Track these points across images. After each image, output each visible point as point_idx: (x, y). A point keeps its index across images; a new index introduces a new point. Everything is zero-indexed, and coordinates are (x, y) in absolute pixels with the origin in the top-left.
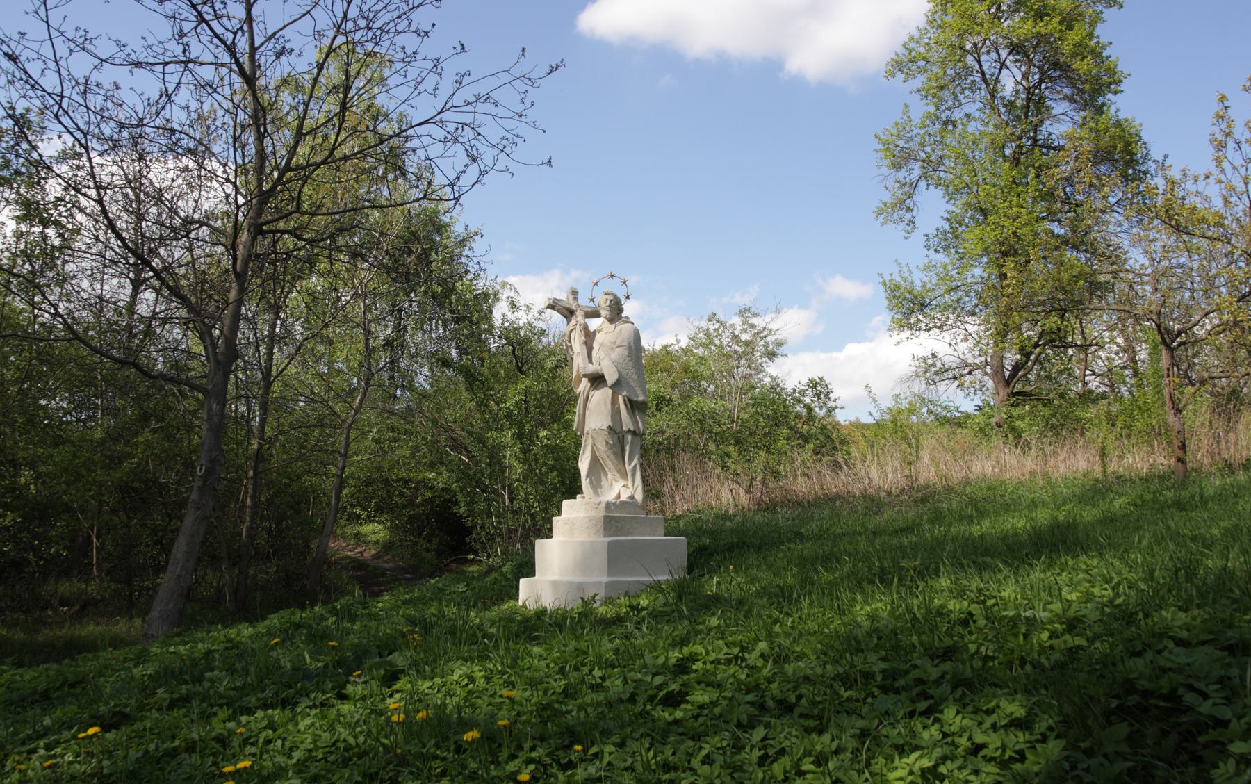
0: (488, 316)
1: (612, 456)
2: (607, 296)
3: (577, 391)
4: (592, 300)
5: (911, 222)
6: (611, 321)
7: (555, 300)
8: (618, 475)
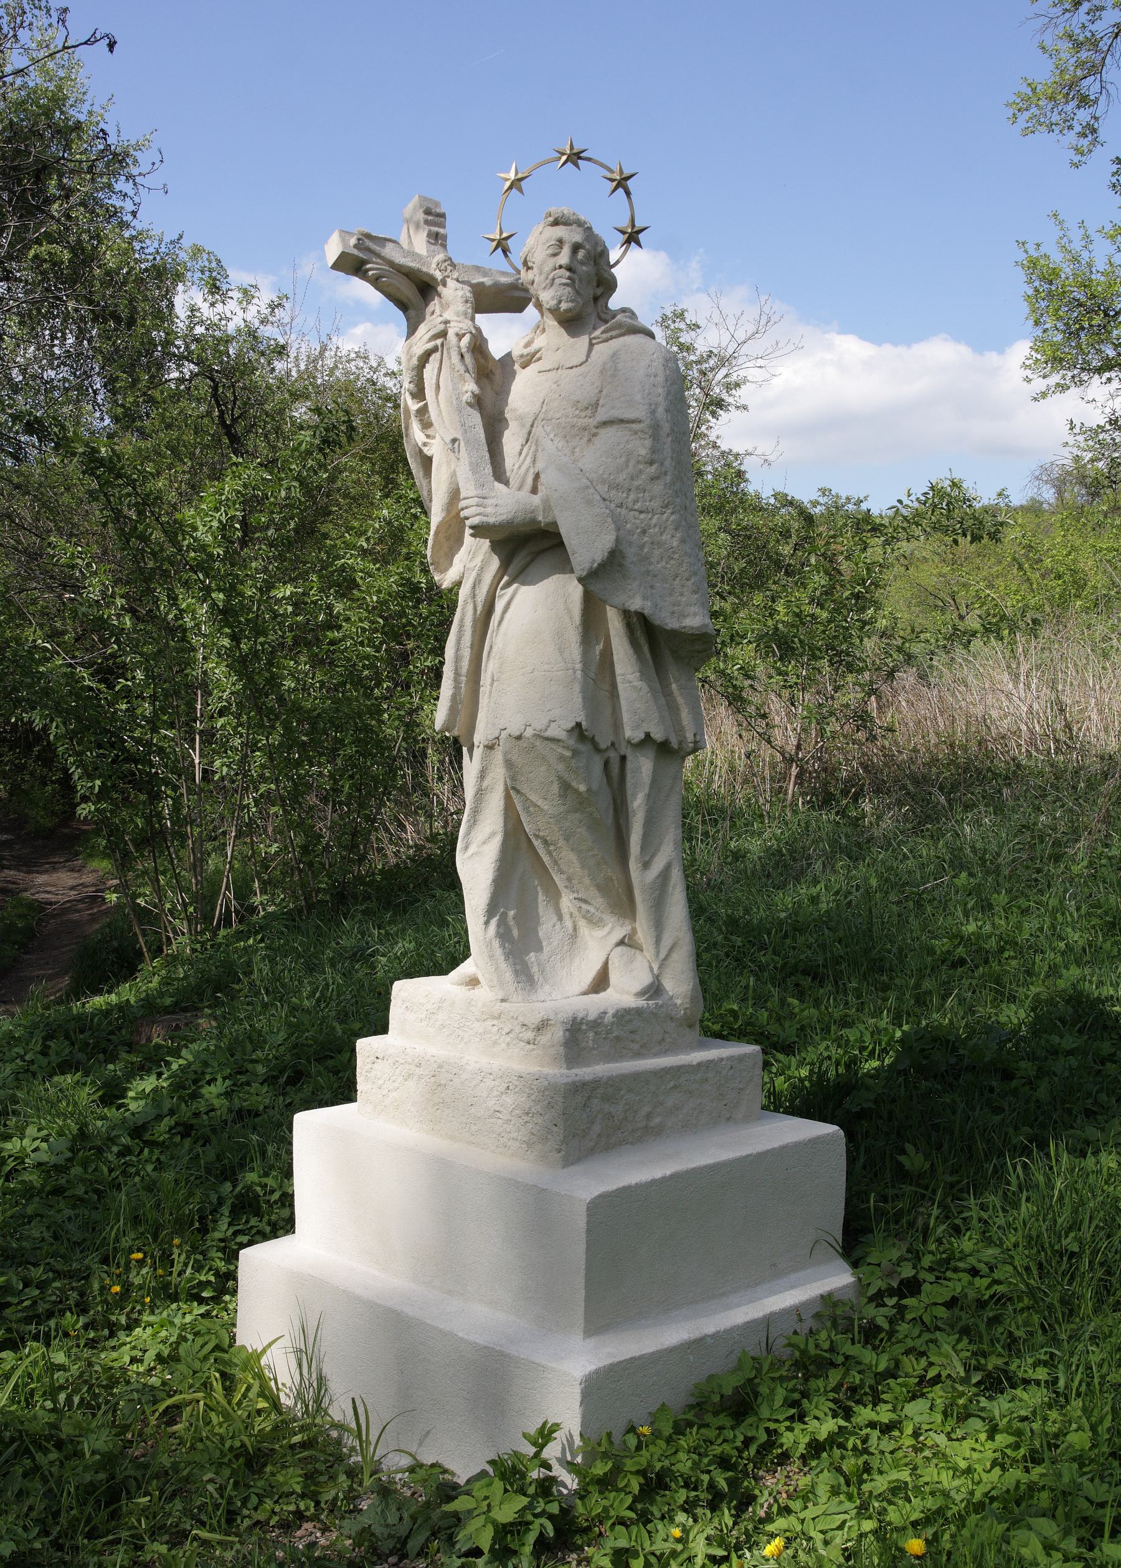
0: (163, 316)
1: (582, 831)
2: (560, 231)
3: (446, 580)
4: (502, 246)
5: (1090, 130)
6: (572, 322)
7: (367, 241)
8: (599, 901)
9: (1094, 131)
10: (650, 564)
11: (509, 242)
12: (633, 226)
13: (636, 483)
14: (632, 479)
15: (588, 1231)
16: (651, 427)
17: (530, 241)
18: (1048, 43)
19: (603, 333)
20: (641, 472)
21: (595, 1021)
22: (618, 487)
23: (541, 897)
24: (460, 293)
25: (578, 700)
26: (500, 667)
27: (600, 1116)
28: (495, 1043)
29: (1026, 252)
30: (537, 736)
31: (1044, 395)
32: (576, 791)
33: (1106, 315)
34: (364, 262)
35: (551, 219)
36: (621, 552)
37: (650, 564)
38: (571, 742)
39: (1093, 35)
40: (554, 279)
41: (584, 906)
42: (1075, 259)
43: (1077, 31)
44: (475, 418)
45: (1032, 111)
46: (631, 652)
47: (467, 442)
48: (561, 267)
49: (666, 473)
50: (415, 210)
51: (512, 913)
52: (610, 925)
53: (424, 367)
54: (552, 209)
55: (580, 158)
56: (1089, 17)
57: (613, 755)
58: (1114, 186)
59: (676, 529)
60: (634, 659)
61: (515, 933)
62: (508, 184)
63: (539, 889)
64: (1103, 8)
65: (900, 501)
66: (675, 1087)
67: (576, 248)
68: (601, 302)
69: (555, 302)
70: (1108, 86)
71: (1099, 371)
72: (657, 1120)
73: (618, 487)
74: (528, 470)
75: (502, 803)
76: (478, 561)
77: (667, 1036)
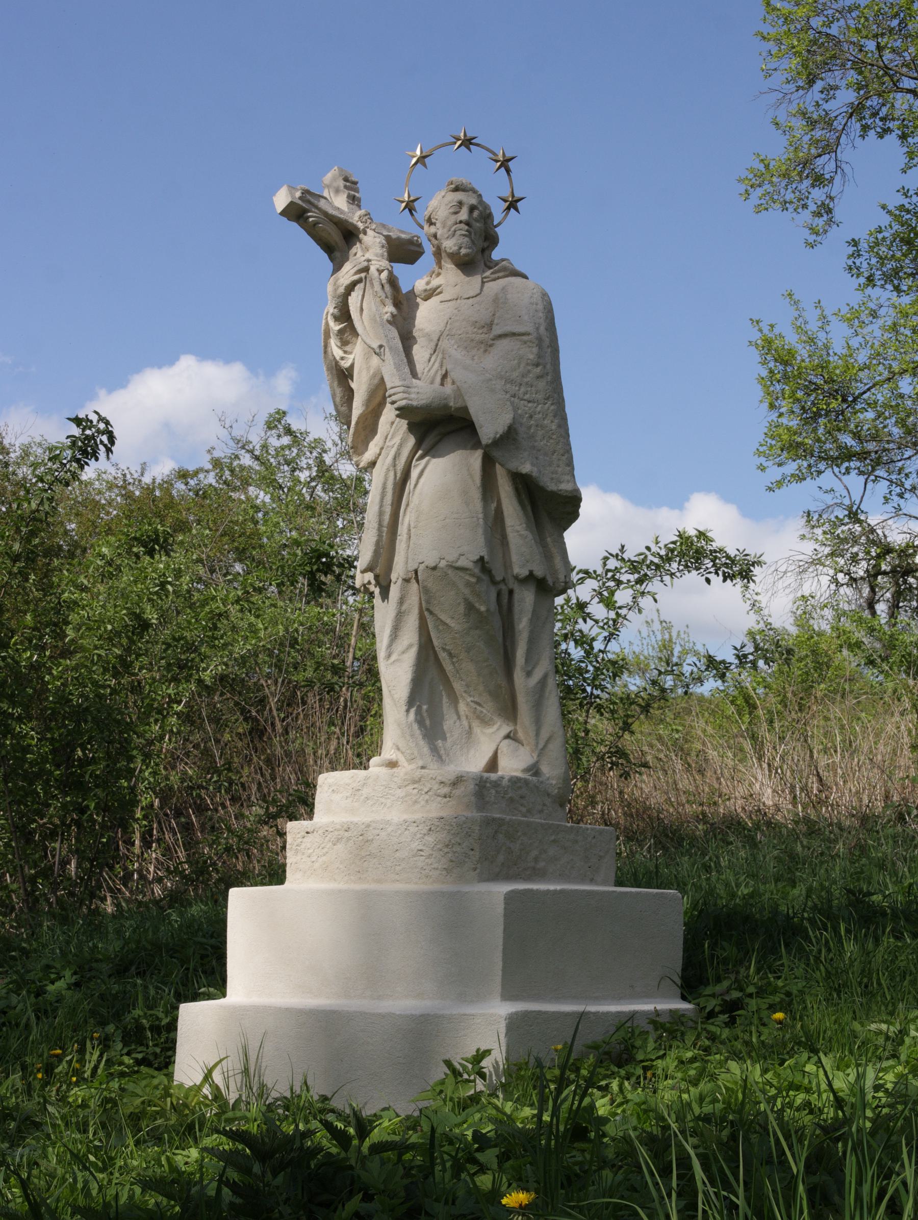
2: (460, 196)
5: (825, 210)
6: (466, 265)
9: (829, 211)
10: (535, 441)
11: (416, 204)
12: (513, 196)
13: (525, 380)
14: (523, 376)
15: (505, 915)
16: (537, 339)
17: (433, 203)
18: (781, 119)
19: (492, 273)
20: (529, 372)
21: (495, 782)
22: (512, 382)
23: (445, 700)
24: (378, 240)
25: (481, 540)
26: (417, 518)
27: (504, 848)
28: (416, 802)
29: (760, 331)
30: (451, 566)
31: (779, 483)
32: (478, 611)
33: (844, 400)
34: (306, 211)
35: (453, 186)
36: (515, 429)
37: (535, 441)
38: (477, 571)
39: (827, 114)
40: (455, 231)
41: (478, 707)
42: (812, 340)
43: (811, 109)
44: (394, 333)
45: (765, 187)
46: (518, 508)
47: (390, 348)
48: (461, 222)
49: (547, 374)
50: (334, 179)
51: (425, 707)
52: (499, 724)
53: (349, 294)
54: (454, 179)
55: (471, 144)
56: (823, 96)
57: (503, 587)
58: (850, 269)
59: (555, 416)
60: (521, 513)
61: (428, 722)
62: (414, 160)
63: (443, 693)
64: (836, 88)
65: (648, 548)
66: (554, 841)
67: (472, 209)
68: (487, 252)
69: (456, 248)
70: (844, 166)
71: (834, 461)
72: (541, 864)
73: (512, 382)
74: (437, 372)
75: (417, 623)
76: (397, 440)
77: (545, 808)
